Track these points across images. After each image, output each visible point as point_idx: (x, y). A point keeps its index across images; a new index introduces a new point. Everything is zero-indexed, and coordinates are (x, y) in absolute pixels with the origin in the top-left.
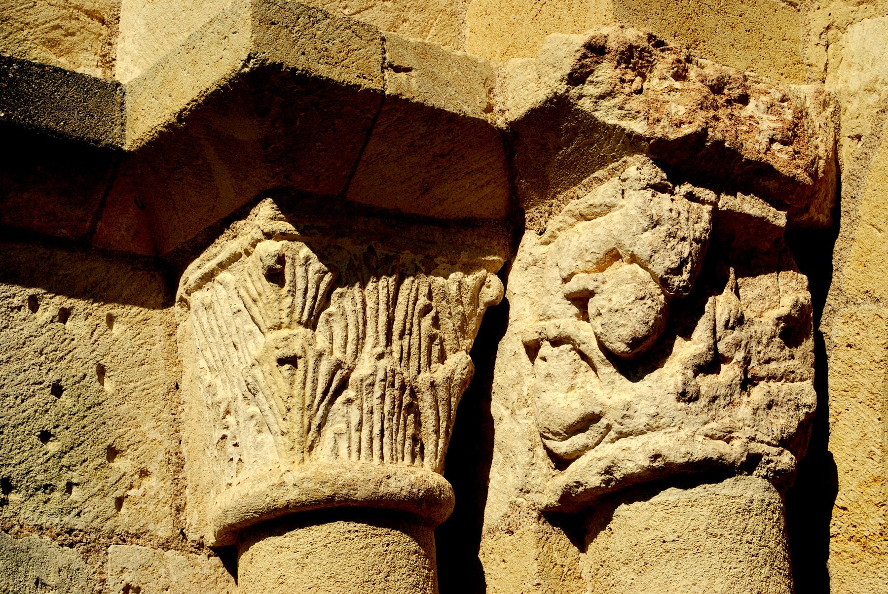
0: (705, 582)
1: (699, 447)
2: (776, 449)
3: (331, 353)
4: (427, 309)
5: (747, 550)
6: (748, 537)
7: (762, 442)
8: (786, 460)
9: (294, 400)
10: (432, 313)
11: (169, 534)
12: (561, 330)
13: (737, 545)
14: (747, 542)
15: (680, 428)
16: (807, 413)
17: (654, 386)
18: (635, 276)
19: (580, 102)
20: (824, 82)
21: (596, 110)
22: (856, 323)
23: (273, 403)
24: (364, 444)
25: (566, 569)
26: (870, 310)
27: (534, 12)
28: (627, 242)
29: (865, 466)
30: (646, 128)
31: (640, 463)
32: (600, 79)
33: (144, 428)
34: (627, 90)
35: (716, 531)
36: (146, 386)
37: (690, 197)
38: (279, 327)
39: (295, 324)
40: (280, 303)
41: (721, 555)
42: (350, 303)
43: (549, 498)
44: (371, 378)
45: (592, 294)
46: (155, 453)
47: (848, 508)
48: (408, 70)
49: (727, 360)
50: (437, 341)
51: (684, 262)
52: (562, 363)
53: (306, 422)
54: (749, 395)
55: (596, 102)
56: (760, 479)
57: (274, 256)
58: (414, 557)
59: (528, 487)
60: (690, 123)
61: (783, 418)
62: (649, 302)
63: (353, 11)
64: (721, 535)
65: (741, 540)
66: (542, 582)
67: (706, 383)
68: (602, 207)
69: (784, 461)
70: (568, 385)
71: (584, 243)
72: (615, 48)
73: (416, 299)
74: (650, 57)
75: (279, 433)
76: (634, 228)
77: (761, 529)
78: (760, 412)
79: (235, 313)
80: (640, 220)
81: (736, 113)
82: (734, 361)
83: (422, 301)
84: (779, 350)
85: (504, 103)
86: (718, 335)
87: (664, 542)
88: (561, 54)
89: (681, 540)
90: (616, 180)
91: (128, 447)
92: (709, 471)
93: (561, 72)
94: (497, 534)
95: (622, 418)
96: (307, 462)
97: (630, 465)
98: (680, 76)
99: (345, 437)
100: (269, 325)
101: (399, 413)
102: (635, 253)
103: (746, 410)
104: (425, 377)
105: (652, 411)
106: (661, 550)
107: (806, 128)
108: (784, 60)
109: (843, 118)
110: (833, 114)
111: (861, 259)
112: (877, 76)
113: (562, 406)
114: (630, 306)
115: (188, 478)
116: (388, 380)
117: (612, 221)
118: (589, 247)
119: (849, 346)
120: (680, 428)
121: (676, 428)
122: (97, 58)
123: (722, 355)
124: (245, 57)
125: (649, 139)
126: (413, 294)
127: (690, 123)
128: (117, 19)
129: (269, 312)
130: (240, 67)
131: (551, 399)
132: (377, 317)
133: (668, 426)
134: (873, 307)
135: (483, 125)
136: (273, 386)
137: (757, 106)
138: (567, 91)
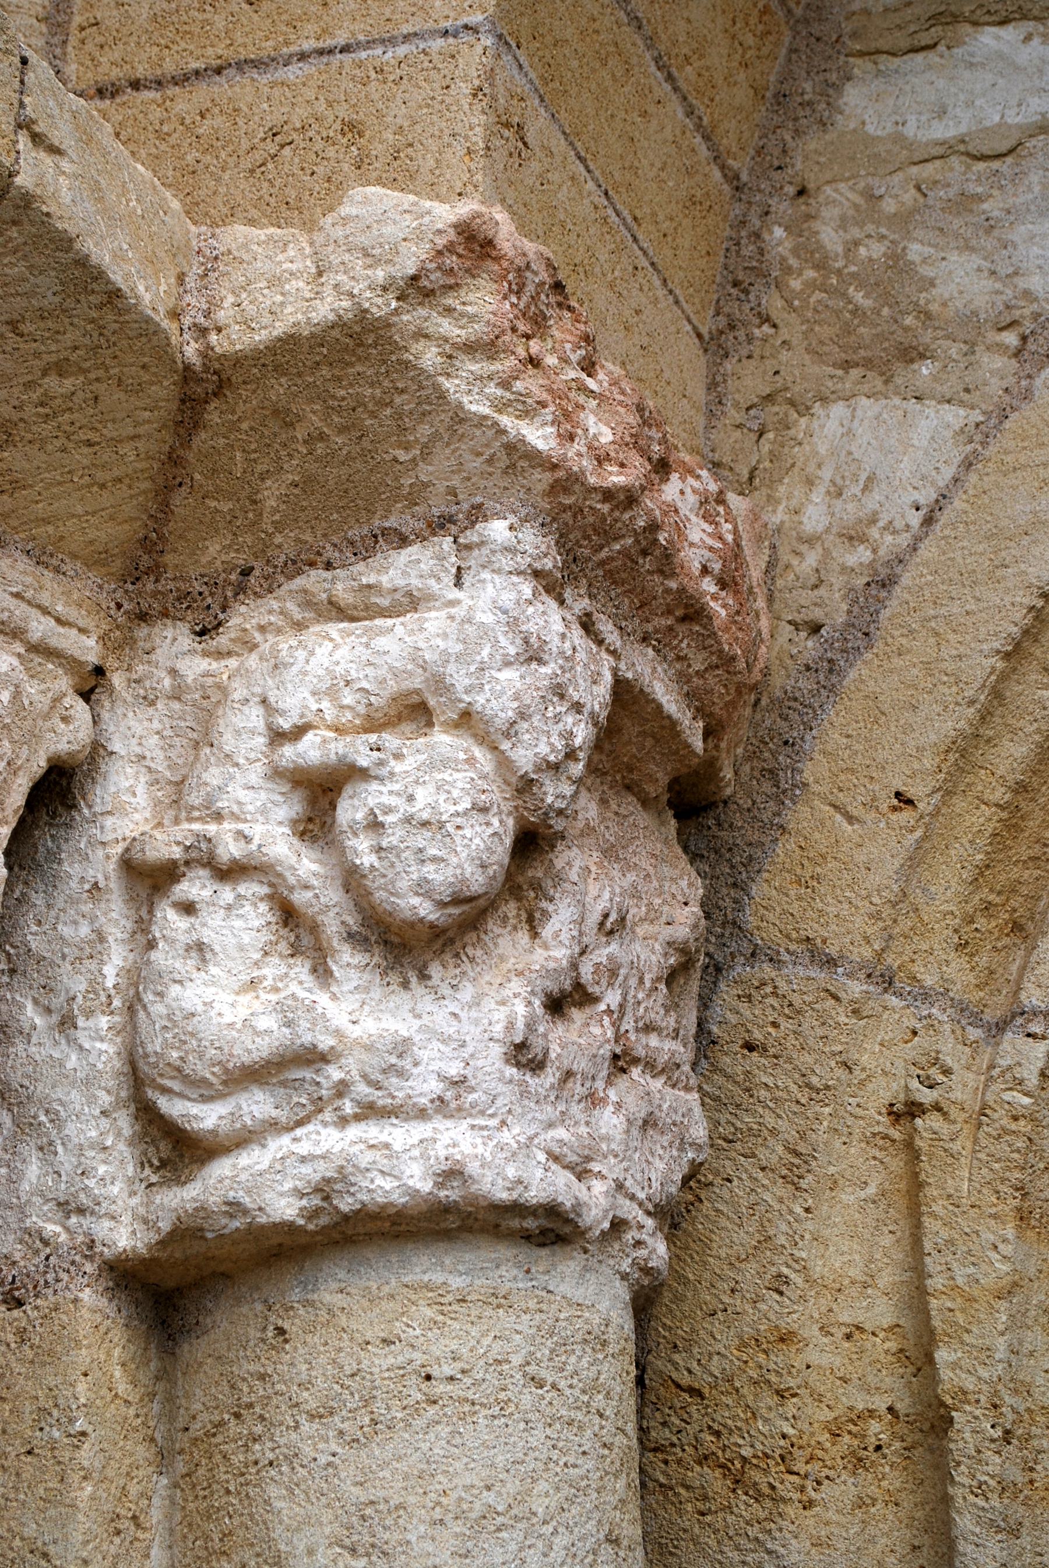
0: (512, 1486)
13: (579, 1415)
15: (503, 1123)
16: (694, 1160)
17: (463, 1015)
19: (419, 346)
27: (258, 156)
28: (460, 678)
29: (762, 1306)
31: (411, 1183)
35: (544, 1374)
37: (587, 624)
41: (548, 1431)
43: (123, 1237)
45: (363, 774)
48: (55, 150)
52: (238, 923)
55: (450, 357)
66: (90, 1429)
70: (245, 978)
71: (343, 665)
80: (501, 638)
82: (602, 1007)
85: (207, 314)
87: (428, 1378)
89: (468, 1381)
92: (549, 1229)
93: (390, 269)
95: (384, 1071)
97: (388, 1184)
103: (615, 1120)
105: (454, 1070)
106: (419, 1396)
112: (875, 513)
114: (459, 820)
117: (421, 629)
118: (354, 674)
119: (750, 1047)
121: (494, 1122)
125: (555, 467)
133: (482, 1113)
134: (820, 975)
138: (396, 312)
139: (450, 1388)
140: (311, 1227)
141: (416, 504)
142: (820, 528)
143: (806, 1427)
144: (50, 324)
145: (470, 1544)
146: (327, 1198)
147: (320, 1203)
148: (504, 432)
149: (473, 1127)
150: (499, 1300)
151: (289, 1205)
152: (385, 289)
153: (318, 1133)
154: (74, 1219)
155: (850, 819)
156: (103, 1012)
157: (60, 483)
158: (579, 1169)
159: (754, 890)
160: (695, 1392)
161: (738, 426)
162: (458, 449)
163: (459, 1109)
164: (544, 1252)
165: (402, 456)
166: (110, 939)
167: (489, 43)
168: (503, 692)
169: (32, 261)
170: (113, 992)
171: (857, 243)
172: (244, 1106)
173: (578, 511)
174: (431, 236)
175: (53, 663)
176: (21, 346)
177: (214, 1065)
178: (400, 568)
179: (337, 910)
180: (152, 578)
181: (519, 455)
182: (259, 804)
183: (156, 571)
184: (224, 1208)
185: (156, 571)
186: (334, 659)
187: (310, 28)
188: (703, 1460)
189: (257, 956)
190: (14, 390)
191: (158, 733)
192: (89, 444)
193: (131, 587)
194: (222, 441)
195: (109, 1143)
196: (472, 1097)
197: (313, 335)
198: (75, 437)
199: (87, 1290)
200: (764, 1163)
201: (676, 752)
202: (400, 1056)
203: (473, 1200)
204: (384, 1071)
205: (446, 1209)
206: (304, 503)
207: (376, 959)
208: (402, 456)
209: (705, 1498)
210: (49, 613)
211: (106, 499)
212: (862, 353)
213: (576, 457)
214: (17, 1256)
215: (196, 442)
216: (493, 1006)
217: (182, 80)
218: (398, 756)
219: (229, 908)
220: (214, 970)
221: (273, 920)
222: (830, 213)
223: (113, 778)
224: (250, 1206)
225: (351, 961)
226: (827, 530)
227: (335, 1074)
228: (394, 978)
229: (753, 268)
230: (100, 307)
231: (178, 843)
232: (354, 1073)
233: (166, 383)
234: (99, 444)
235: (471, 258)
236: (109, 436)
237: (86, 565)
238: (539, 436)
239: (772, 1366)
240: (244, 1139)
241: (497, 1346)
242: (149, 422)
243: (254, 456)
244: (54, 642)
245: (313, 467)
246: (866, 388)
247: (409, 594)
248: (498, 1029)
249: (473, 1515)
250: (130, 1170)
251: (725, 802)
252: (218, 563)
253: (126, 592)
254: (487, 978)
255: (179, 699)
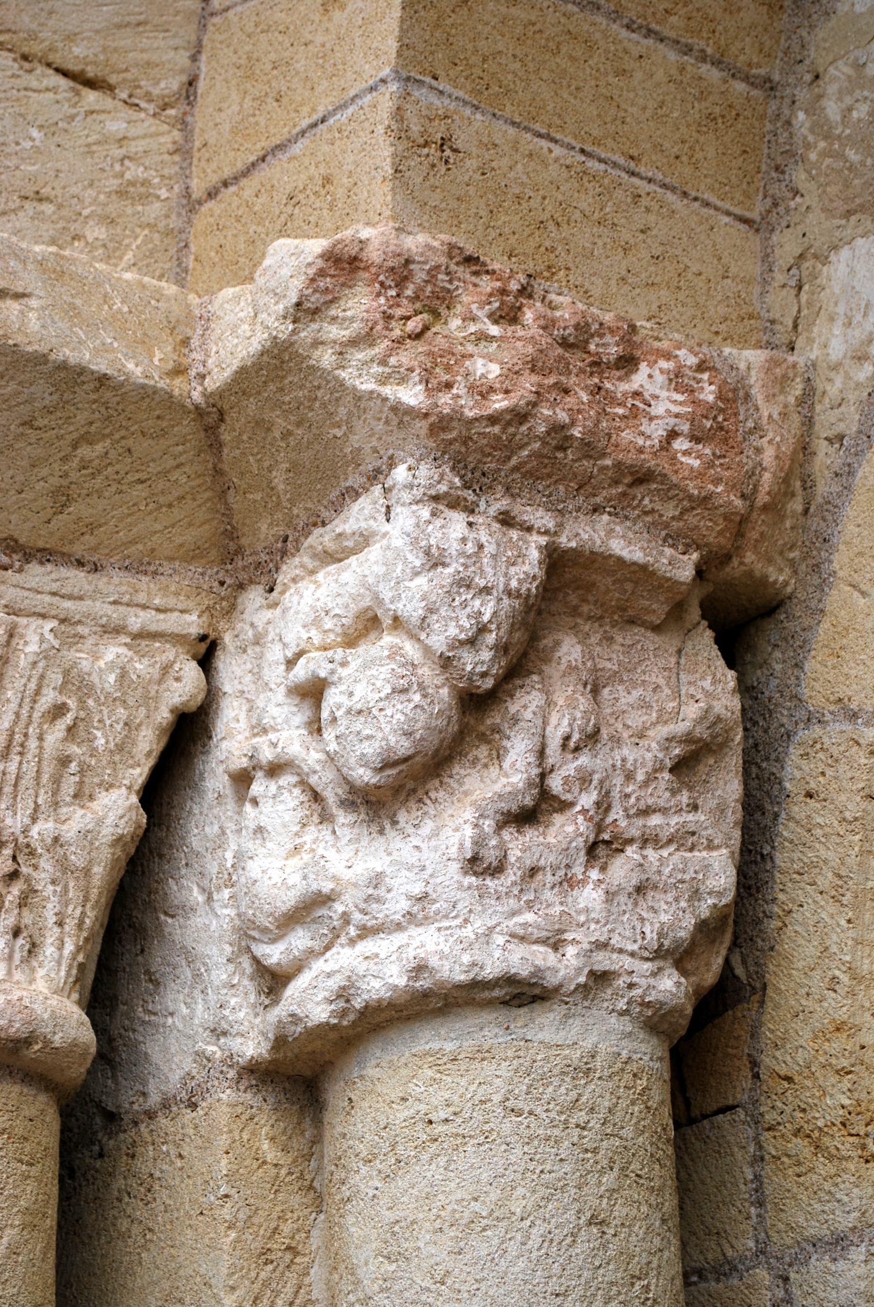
1: (497, 955)
2: (648, 965)
4: (59, 710)
5: (575, 1139)
6: (581, 1117)
7: (621, 951)
8: (669, 985)
12: (279, 750)
13: (556, 1132)
14: (578, 1126)
15: (466, 921)
16: (715, 905)
17: (424, 846)
18: (395, 652)
19: (317, 353)
20: (793, 349)
22: (821, 755)
25: (283, 1172)
26: (842, 732)
30: (421, 398)
31: (391, 981)
32: (349, 313)
34: (397, 333)
35: (520, 1105)
37: (506, 520)
41: (526, 1149)
43: (252, 1047)
47: (796, 1078)
49: (565, 806)
50: (73, 767)
51: (483, 629)
52: (281, 807)
54: (603, 869)
55: (341, 353)
56: (613, 1019)
60: (507, 392)
61: (519, 859)
62: (417, 698)
64: (531, 1113)
65: (566, 1121)
67: (520, 846)
68: (356, 537)
69: (662, 987)
71: (323, 600)
72: (378, 261)
73: (38, 692)
74: (450, 282)
76: (398, 570)
77: (607, 1104)
78: (622, 898)
81: (608, 385)
82: (578, 808)
83: (49, 697)
84: (667, 794)
86: (550, 761)
87: (430, 1122)
88: (286, 272)
89: (459, 1120)
90: (377, 490)
94: (174, 1109)
95: (366, 901)
97: (376, 984)
98: (508, 316)
102: (399, 613)
103: (594, 895)
104: (44, 828)
105: (417, 889)
107: (741, 418)
108: (722, 310)
109: (818, 408)
110: (801, 402)
111: (832, 645)
113: (273, 882)
118: (330, 605)
119: (809, 795)
120: (466, 921)
121: (458, 922)
123: (555, 798)
125: (426, 415)
126: (32, 686)
127: (507, 392)
131: (259, 871)
133: (446, 917)
134: (847, 727)
137: (650, 376)
139: (445, 1127)
140: (345, 1023)
142: (841, 356)
143: (864, 1096)
144: (59, 414)
145: (462, 1244)
146: (348, 1001)
148: (385, 399)
149: (439, 929)
150: (483, 1054)
151: (324, 1010)
152: (285, 318)
154: (222, 1040)
155: (864, 594)
156: (226, 886)
158: (552, 941)
159: (807, 667)
160: (789, 1079)
161: (784, 286)
163: (426, 918)
164: (525, 1009)
167: (394, 88)
168: (413, 597)
171: (850, 109)
173: (466, 440)
178: (360, 515)
181: (401, 413)
187: (305, 110)
188: (797, 1133)
189: (297, 828)
192: (141, 482)
195: (235, 981)
196: (434, 907)
197: (254, 364)
200: (821, 888)
201: (660, 586)
202: (376, 887)
203: (441, 984)
204: (366, 901)
205: (426, 995)
207: (362, 816)
209: (799, 1164)
211: (177, 513)
212: (858, 201)
213: (459, 400)
216: (451, 833)
217: (246, 173)
218: (344, 664)
219: (274, 797)
220: (269, 845)
221: (306, 799)
222: (832, 89)
223: (226, 711)
226: (845, 357)
227: (339, 908)
228: (374, 828)
229: (786, 152)
238: (411, 395)
239: (833, 1052)
240: (298, 967)
241: (481, 1091)
244: (153, 628)
245: (293, 455)
246: (860, 231)
247: (361, 534)
248: (453, 851)
249: (464, 1222)
250: (252, 998)
251: (790, 598)
254: (450, 812)
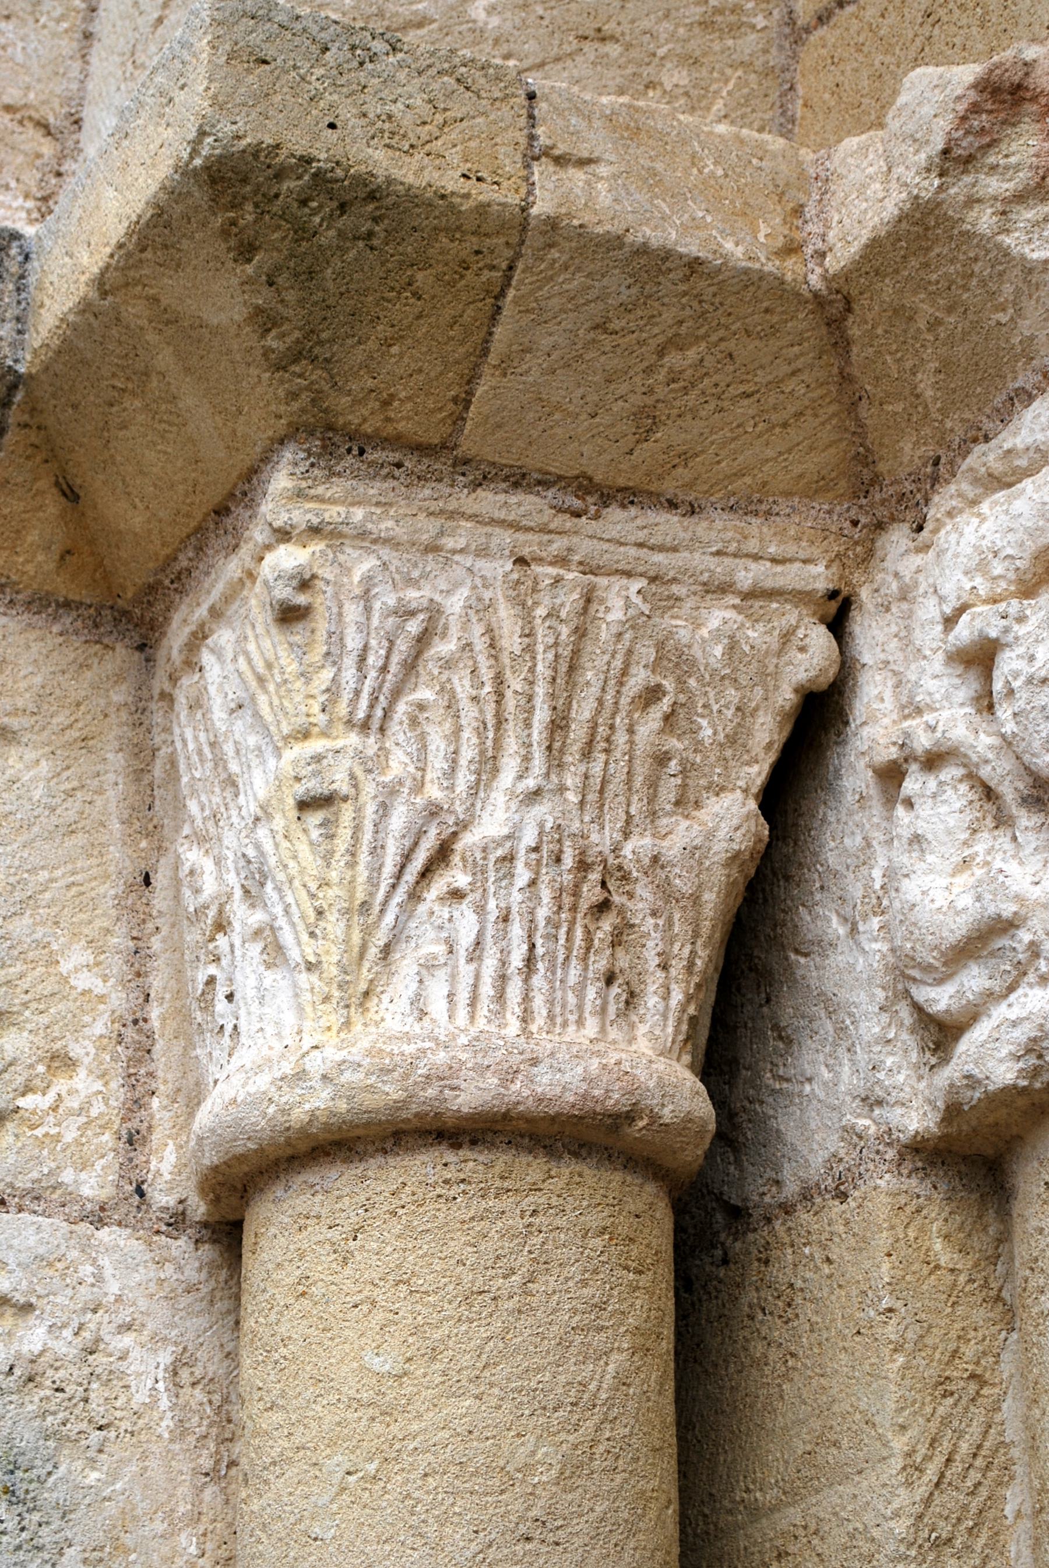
3: (419, 786)
9: (331, 893)
10: (665, 704)
11: (107, 1193)
21: (1008, 231)
23: (290, 899)
24: (487, 989)
32: (1013, 160)
33: (65, 967)
36: (78, 878)
38: (306, 735)
39: (341, 727)
40: (308, 681)
42: (467, 683)
43: (916, 1119)
44: (508, 844)
46: (87, 1019)
52: (943, 809)
53: (356, 938)
57: (292, 577)
58: (598, 1243)
59: (879, 1092)
63: (526, 63)
66: (899, 1305)
68: (1031, 454)
71: (989, 538)
73: (625, 672)
75: (303, 967)
79: (233, 711)
83: (639, 678)
85: (823, 237)
88: (927, 110)
91: (25, 1005)
96: (357, 1028)
99: (442, 974)
100: (286, 730)
101: (572, 923)
104: (638, 845)
113: (937, 905)
115: (160, 1074)
116: (548, 851)
118: (999, 544)
122: (30, 204)
124: (192, 135)
126: (618, 663)
128: (76, 122)
129: (286, 703)
130: (185, 156)
131: (918, 891)
132: (531, 711)
135: (779, 290)
136: (292, 864)
140: (1038, 1085)
141: (1032, 359)
144: (640, 313)
147: (1037, 1062)
151: (1009, 1069)
153: (1026, 995)
156: (875, 914)
157: (734, 439)
162: (1039, 297)
165: (1003, 318)
166: (874, 843)
169: (589, 270)
170: (880, 893)
172: (966, 983)
174: (952, 105)
175: (778, 602)
176: (620, 341)
177: (932, 950)
179: (1009, 778)
180: (877, 488)
182: (943, 690)
183: (876, 480)
184: (965, 1082)
185: (876, 480)
186: (980, 534)
189: (964, 836)
190: (635, 379)
191: (896, 636)
193: (864, 501)
194: (870, 350)
195: (891, 1035)
197: (889, 234)
198: (726, 395)
199: (887, 1176)
206: (952, 386)
208: (1003, 318)
210: (761, 558)
214: (842, 1153)
215: (854, 358)
218: (1021, 619)
219: (934, 796)
220: (930, 858)
224: (981, 1076)
225: (1027, 824)
230: (687, 278)
231: (894, 744)
232: (1040, 932)
233: (801, 316)
234: (758, 391)
235: (1005, 109)
236: (764, 381)
237: (807, 496)
242: (802, 354)
243: (899, 355)
244: (769, 584)
245: (943, 351)
250: (914, 1056)
252: (916, 459)
253: (861, 507)
255: (905, 599)
